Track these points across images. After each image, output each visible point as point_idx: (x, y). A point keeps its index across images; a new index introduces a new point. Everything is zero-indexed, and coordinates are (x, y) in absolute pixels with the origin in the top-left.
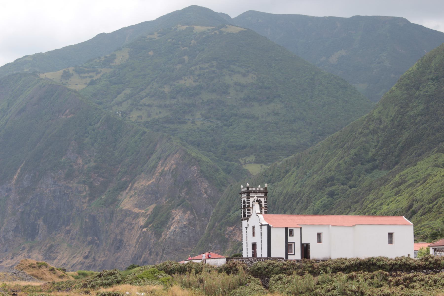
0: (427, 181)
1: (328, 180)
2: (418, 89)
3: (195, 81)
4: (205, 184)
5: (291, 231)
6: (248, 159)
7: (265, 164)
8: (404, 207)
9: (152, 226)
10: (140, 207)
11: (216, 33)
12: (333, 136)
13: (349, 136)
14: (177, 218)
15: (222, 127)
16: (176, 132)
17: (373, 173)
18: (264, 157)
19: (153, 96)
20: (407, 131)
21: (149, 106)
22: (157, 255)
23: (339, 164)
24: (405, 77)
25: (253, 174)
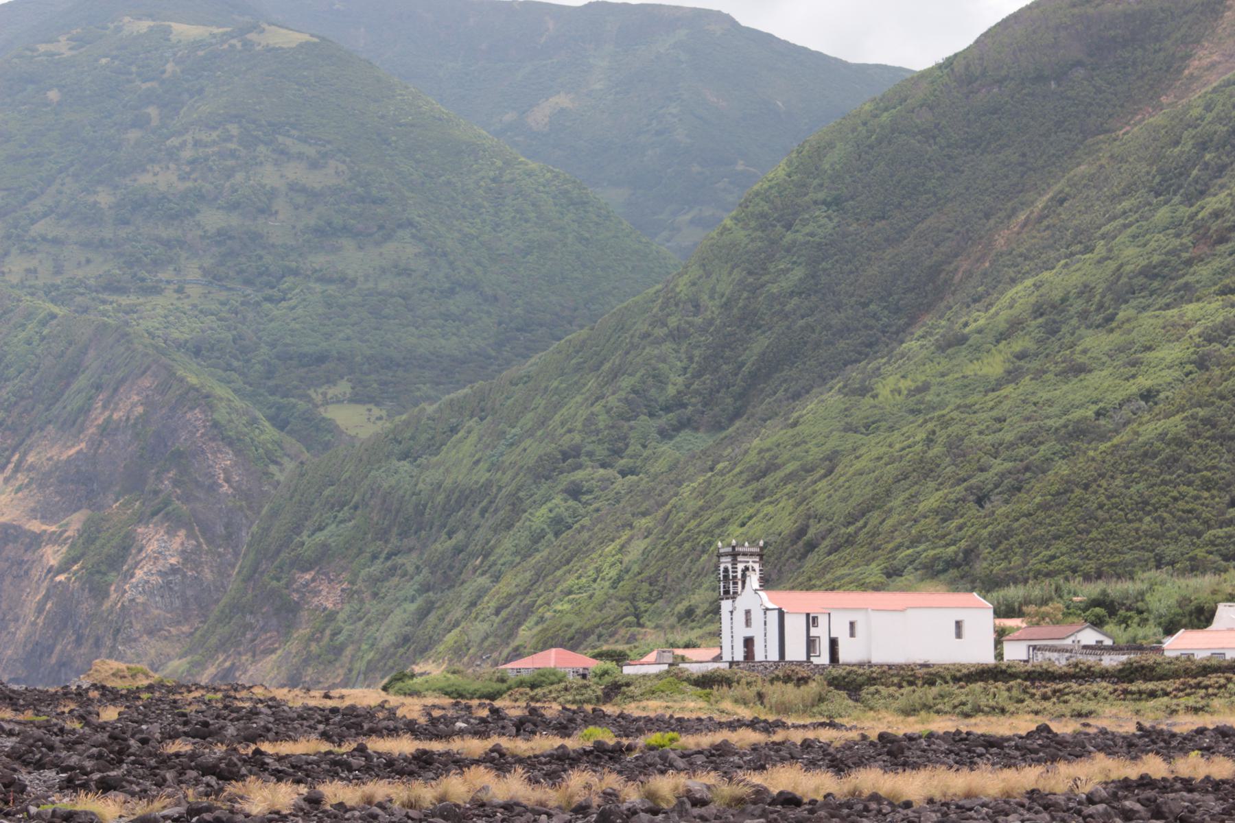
0: (839, 469)
1: (565, 456)
2: (789, 227)
3: (182, 178)
4: (227, 459)
5: (815, 619)
6: (331, 392)
7: (377, 404)
8: (786, 532)
9: (82, 568)
10: (45, 519)
11: (232, 46)
12: (570, 341)
13: (612, 340)
14: (153, 547)
15: (258, 304)
16: (135, 316)
17: (678, 439)
18: (375, 385)
19: (65, 216)
20: (764, 332)
21: (56, 241)
22: (98, 643)
23: (592, 414)
24: (757, 194)
25: (349, 432)
